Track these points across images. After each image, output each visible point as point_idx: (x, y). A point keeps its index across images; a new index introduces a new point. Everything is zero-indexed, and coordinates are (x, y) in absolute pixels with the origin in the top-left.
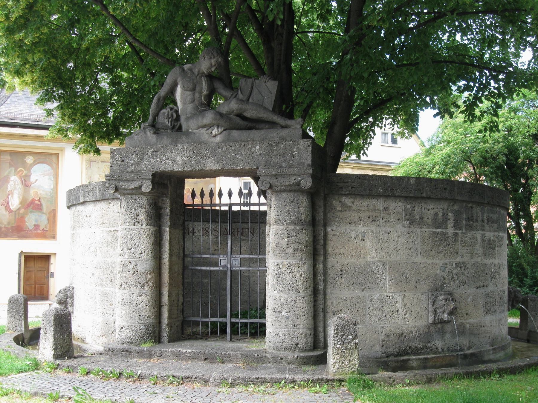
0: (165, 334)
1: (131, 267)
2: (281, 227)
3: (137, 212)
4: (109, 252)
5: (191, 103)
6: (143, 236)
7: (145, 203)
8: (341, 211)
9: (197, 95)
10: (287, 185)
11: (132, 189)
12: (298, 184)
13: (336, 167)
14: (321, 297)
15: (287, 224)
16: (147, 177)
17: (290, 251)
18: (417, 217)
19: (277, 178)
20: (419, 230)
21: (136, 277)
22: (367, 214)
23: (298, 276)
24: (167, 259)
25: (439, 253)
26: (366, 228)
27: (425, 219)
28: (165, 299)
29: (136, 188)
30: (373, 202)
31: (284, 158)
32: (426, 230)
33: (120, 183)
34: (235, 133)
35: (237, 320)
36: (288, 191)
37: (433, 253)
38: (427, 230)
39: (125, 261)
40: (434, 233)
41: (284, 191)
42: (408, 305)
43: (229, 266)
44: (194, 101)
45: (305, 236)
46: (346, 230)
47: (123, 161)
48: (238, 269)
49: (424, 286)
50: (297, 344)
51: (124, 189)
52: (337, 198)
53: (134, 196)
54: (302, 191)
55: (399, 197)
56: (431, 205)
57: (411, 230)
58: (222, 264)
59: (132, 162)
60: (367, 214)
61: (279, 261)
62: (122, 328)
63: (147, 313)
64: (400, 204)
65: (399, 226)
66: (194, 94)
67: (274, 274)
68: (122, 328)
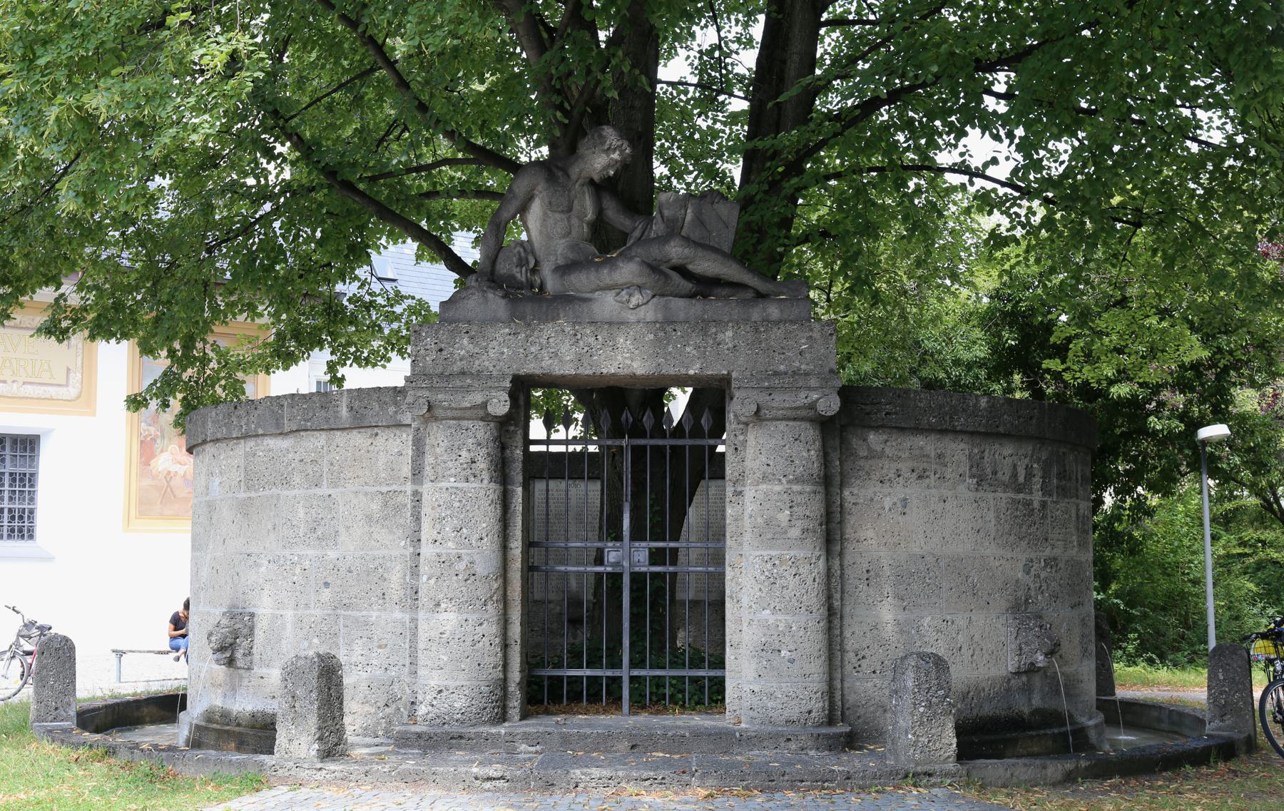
0: (515, 703)
1: (461, 566)
2: (778, 488)
4: (375, 536)
5: (564, 236)
6: (485, 503)
8: (866, 458)
9: (575, 221)
11: (466, 408)
12: (812, 406)
14: (836, 622)
15: (789, 482)
17: (795, 533)
18: (989, 470)
20: (991, 495)
21: (473, 587)
22: (910, 464)
23: (810, 581)
24: (520, 550)
25: (1021, 539)
26: (907, 491)
27: (1000, 474)
28: (516, 630)
30: (920, 441)
32: (1001, 495)
35: (642, 673)
36: (789, 419)
37: (1012, 538)
38: (1004, 496)
39: (448, 554)
40: (1013, 500)
41: (785, 419)
42: (977, 638)
43: (626, 564)
44: (570, 233)
45: (816, 507)
46: (875, 493)
47: (441, 350)
48: (644, 569)
49: (1001, 603)
50: (810, 712)
51: (445, 409)
52: (859, 432)
53: (465, 423)
54: (487, 418)
55: (962, 432)
56: (1008, 449)
57: (979, 495)
58: (612, 560)
59: (463, 353)
60: (910, 464)
61: (773, 553)
62: (440, 691)
63: (492, 659)
64: (962, 446)
65: (961, 488)
66: (569, 219)
67: (763, 578)
68: (440, 691)
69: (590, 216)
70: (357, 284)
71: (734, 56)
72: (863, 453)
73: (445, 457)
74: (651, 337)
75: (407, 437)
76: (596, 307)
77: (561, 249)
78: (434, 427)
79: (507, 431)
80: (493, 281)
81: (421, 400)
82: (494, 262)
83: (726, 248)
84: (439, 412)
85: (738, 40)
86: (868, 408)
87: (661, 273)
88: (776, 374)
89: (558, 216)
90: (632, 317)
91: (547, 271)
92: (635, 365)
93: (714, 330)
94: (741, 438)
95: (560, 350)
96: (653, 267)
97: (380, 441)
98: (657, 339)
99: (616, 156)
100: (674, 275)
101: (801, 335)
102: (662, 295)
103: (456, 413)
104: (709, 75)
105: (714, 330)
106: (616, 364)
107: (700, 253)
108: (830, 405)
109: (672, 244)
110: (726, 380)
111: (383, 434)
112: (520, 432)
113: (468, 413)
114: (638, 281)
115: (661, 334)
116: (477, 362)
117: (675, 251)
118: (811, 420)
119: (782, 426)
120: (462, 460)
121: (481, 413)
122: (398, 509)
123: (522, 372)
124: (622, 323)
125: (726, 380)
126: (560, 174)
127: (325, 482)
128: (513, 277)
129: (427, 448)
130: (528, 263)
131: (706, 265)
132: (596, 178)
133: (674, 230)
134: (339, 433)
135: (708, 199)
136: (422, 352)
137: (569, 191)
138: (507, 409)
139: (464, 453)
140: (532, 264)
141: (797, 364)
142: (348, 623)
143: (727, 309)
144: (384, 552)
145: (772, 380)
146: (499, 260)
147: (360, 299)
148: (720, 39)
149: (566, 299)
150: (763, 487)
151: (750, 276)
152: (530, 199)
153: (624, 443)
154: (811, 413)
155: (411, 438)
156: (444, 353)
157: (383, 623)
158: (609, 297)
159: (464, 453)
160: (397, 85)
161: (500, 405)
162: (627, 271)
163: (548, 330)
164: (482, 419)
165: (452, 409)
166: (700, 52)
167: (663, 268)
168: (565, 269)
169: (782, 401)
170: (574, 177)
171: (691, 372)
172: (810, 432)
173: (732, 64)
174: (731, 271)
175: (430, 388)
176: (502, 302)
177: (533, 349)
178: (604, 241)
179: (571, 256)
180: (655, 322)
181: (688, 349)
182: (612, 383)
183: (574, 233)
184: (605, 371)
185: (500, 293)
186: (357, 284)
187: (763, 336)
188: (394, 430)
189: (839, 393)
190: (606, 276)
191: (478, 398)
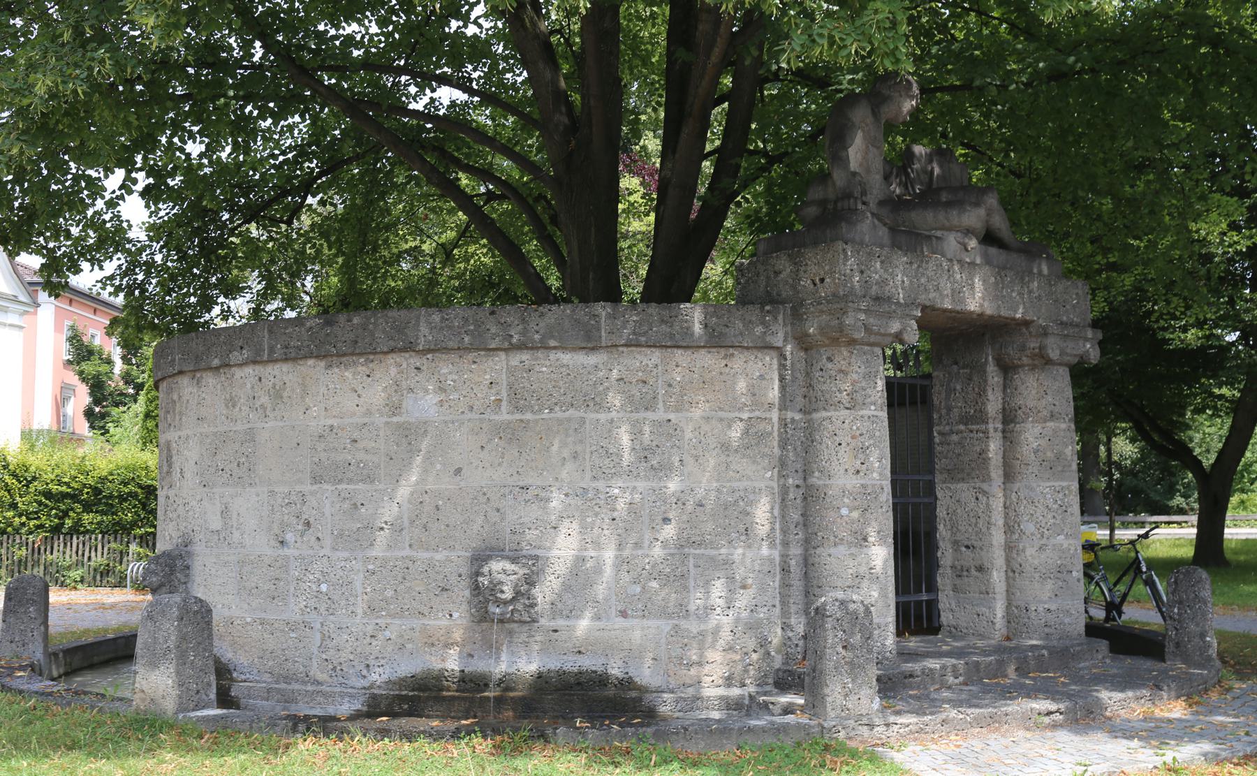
2: (1063, 426)
39: (873, 486)
61: (1065, 484)
67: (1056, 506)
98: (996, 283)
122: (763, 436)
127: (661, 405)
134: (680, 351)
142: (701, 563)
144: (745, 483)
150: (1051, 424)
157: (748, 561)
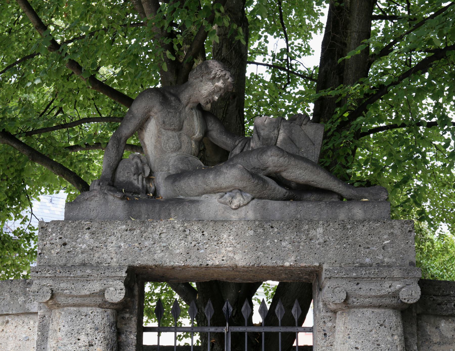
3: (90, 338)
7: (103, 322)
8: (439, 343)
9: (185, 138)
10: (376, 297)
11: (85, 296)
12: (395, 295)
13: (279, 286)
16: (119, 274)
19: (358, 284)
29: (92, 295)
31: (368, 250)
33: (62, 285)
34: (275, 206)
36: (375, 307)
44: (180, 148)
47: (65, 244)
51: (67, 297)
52: (432, 321)
53: (84, 310)
59: (84, 246)
69: (198, 134)
70: (20, 220)
71: (297, 59)
72: (436, 339)
73: (65, 341)
74: (251, 232)
75: (33, 324)
76: (203, 208)
77: (172, 161)
78: (56, 313)
79: (123, 318)
80: (113, 186)
81: (45, 289)
82: (115, 170)
83: (315, 157)
84: (61, 300)
85: (300, 49)
86: (440, 299)
87: (259, 178)
88: (362, 265)
89: (170, 133)
90: (234, 217)
91: (160, 179)
92: (237, 257)
93: (306, 227)
94: (329, 324)
95: (172, 245)
96: (254, 174)
97: (10, 328)
98: (257, 235)
99: (220, 84)
100: (272, 183)
101: (383, 231)
102: (260, 198)
103: (76, 301)
104: (279, 74)
105: (306, 227)
106: (220, 257)
107: (293, 162)
108: (412, 294)
109: (269, 153)
110: (316, 273)
111: (13, 322)
112: (134, 319)
113: (88, 301)
114: (240, 185)
115: (260, 230)
116: (97, 255)
117: (272, 160)
118: (394, 308)
119: (368, 312)
120: (81, 343)
121: (99, 300)
123: (136, 264)
124: (226, 221)
125: (316, 273)
126: (173, 98)
128: (131, 183)
129: (50, 333)
130: (144, 172)
131: (298, 173)
132: (203, 102)
133: (268, 144)
135: (297, 122)
136: (48, 246)
137: (180, 113)
138: (122, 296)
139: (83, 337)
140: (147, 173)
141: (381, 257)
143: (317, 209)
145: (359, 272)
146: (119, 170)
147: (22, 232)
148: (288, 45)
149: (176, 201)
151: (336, 183)
152: (146, 119)
153: (225, 330)
154: (394, 301)
155: (37, 324)
156: (67, 247)
158: (214, 199)
159: (83, 337)
160: (37, 28)
161: (116, 293)
162: (230, 175)
163: (161, 227)
164: (100, 306)
165: (73, 296)
166: (273, 55)
167: (261, 175)
168: (175, 178)
169: (369, 290)
170: (184, 101)
171: (287, 264)
172: (393, 319)
173: (296, 65)
174: (320, 179)
175: (54, 278)
176: (121, 203)
177: (146, 243)
178: (211, 156)
179: (181, 167)
180: (255, 221)
181: (284, 244)
182: (215, 277)
183: (184, 148)
184: (210, 263)
185: (119, 195)
186: (20, 220)
187: (350, 233)
188: (23, 317)
189: (419, 283)
190: (212, 180)
191: (96, 287)
